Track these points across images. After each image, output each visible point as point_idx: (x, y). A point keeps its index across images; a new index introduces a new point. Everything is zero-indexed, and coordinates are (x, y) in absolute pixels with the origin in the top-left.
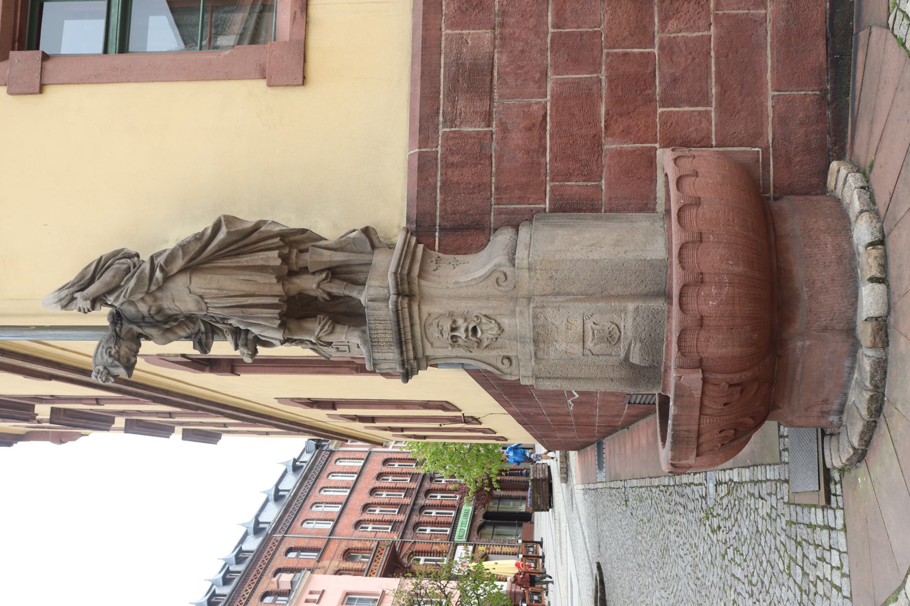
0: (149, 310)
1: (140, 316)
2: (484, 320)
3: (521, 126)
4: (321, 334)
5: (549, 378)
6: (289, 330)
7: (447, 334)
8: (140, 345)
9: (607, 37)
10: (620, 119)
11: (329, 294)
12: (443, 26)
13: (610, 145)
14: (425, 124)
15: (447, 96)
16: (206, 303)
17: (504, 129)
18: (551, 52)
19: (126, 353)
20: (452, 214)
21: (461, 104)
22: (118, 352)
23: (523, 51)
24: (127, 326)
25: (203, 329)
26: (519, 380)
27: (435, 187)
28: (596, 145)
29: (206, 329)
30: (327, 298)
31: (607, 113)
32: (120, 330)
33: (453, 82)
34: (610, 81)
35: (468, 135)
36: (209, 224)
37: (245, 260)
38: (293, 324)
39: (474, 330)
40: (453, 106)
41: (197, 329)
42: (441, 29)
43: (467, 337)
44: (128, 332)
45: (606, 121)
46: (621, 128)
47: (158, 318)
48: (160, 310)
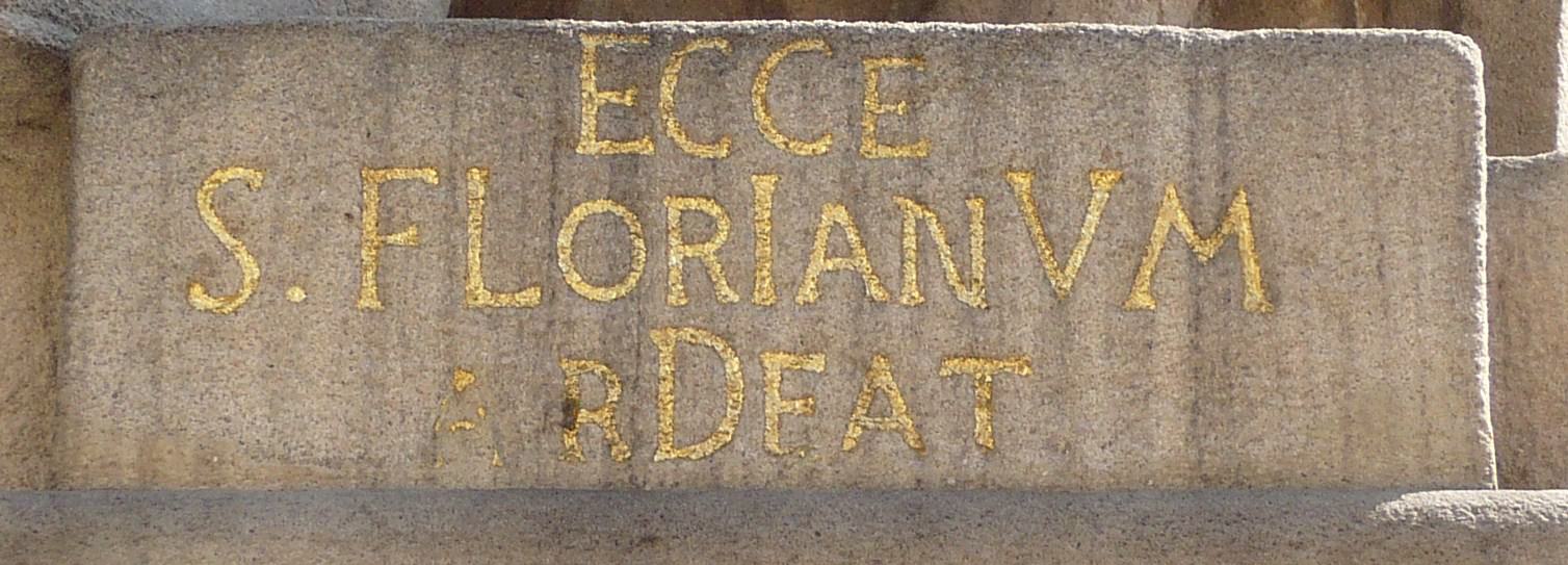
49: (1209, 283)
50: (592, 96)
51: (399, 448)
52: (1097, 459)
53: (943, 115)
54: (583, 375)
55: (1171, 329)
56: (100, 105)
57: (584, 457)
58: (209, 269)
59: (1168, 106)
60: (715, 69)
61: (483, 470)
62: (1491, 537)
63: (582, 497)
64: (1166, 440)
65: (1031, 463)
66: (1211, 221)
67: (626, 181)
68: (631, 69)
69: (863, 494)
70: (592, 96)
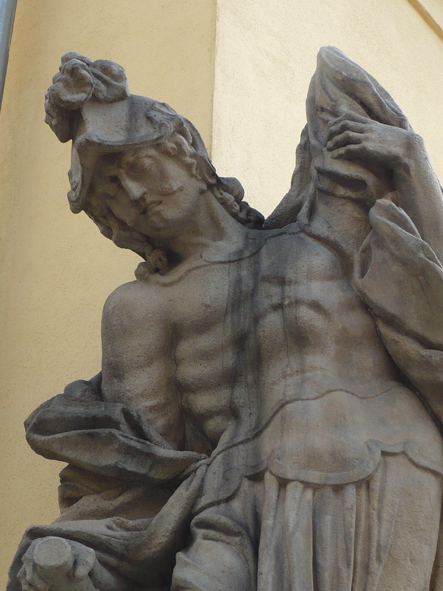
0: (316, 306)
1: (290, 274)
16: (338, 489)
19: (163, 176)
22: (177, 155)
24: (234, 237)
29: (157, 461)
41: (153, 433)
44: (215, 221)
47: (272, 322)
48: (299, 339)
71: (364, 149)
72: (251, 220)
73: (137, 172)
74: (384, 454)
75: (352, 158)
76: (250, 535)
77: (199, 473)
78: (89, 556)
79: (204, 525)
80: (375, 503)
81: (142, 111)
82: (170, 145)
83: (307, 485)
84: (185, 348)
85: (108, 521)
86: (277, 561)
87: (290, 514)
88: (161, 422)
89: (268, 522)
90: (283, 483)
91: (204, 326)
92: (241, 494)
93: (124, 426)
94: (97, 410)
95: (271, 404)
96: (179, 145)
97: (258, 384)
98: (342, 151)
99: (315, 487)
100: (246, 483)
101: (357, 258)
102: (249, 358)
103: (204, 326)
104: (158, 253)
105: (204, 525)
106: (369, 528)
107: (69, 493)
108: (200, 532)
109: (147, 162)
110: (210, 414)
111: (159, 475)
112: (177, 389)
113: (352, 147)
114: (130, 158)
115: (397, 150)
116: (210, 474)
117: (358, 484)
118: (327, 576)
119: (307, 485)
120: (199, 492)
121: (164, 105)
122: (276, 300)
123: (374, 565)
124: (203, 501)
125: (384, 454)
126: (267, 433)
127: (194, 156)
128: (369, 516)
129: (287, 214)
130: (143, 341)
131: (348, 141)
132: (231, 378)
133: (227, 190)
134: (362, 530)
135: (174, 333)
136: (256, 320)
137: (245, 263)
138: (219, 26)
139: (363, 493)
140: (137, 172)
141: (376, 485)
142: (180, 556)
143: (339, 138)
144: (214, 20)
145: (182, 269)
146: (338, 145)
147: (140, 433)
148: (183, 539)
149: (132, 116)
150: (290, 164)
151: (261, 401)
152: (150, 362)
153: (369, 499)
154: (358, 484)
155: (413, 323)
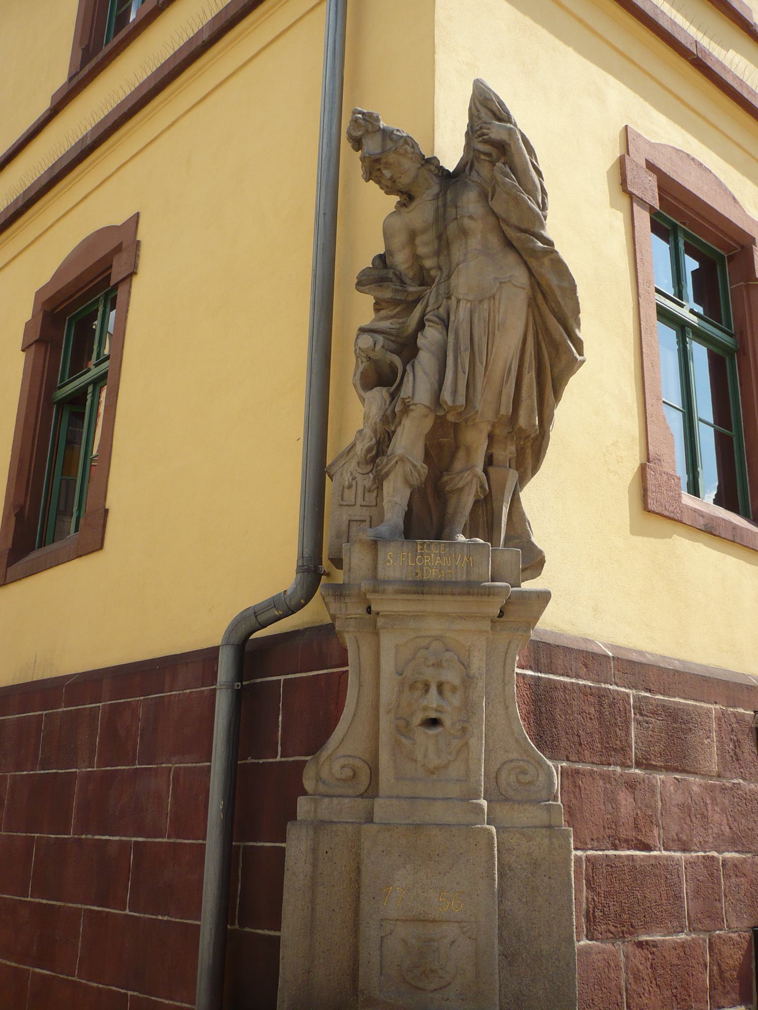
2: (456, 743)
3: (639, 812)
4: (409, 465)
5: (314, 850)
6: (426, 416)
7: (429, 674)
8: (389, 191)
9: (719, 936)
10: (649, 964)
11: (461, 490)
12: (718, 707)
13: (620, 950)
14: (634, 669)
15: (664, 707)
17: (631, 785)
18: (703, 857)
20: (551, 698)
21: (656, 723)
23: (703, 816)
25: (411, 289)
26: (305, 793)
27: (578, 677)
28: (623, 930)
30: (447, 488)
31: (655, 944)
32: (430, 171)
33: (673, 714)
34: (683, 945)
35: (628, 734)
36: (583, 333)
37: (530, 377)
38: (428, 423)
39: (434, 722)
40: (654, 713)
41: (408, 281)
42: (716, 703)
43: (425, 709)
45: (647, 942)
46: (641, 967)
47: (452, 227)
49: (468, 563)
50: (419, 547)
51: (404, 577)
52: (459, 579)
53: (447, 549)
54: (418, 571)
55: (465, 568)
56: (379, 546)
57: (418, 578)
58: (389, 561)
59: (465, 549)
60: (429, 545)
61: (410, 579)
62: (179, 1007)
63: (700, 926)
64: (464, 577)
65: (454, 580)
66: (468, 559)
67: (422, 554)
68: (422, 544)
69: (440, 582)
70: (419, 547)
71: (490, 138)
72: (445, 176)
73: (388, 165)
74: (501, 283)
75: (485, 142)
76: (445, 323)
77: (426, 297)
78: (380, 339)
79: (429, 320)
80: (497, 304)
81: (387, 134)
82: (402, 151)
83: (468, 301)
84: (418, 241)
85: (391, 321)
86: (530, 279)
87: (461, 315)
88: (411, 274)
89: (452, 318)
90: (458, 301)
91: (424, 231)
92: (443, 306)
93: (394, 279)
94: (383, 272)
95: (454, 264)
96: (406, 151)
97: (449, 255)
98: (481, 139)
99: (471, 302)
100: (445, 300)
101: (490, 190)
102: (443, 245)
103: (424, 231)
104: (405, 196)
105: (429, 320)
106: (494, 317)
107: (378, 307)
108: (427, 323)
109: (392, 160)
110: (431, 269)
111: (410, 298)
112: (416, 258)
113: (485, 137)
114: (384, 160)
115: (504, 136)
116: (431, 296)
117: (489, 298)
118: (476, 339)
119: (468, 301)
120: (427, 306)
121: (398, 130)
122: (454, 216)
123: (496, 332)
124: (428, 309)
125: (501, 283)
126: (453, 277)
127: (413, 153)
128: (494, 311)
129: (465, 167)
130: (399, 240)
131: (483, 135)
132: (438, 253)
133: (431, 163)
134: (491, 318)
135: (412, 236)
136: (446, 227)
137: (440, 199)
138: (436, 56)
139: (492, 301)
140: (388, 165)
141: (497, 297)
142: (419, 334)
143: (479, 132)
144: (434, 53)
145: (414, 204)
146: (479, 136)
147: (403, 282)
148: (421, 326)
149: (384, 139)
150: (462, 142)
151: (450, 262)
152: (404, 248)
153: (494, 304)
154: (489, 298)
155: (514, 220)
